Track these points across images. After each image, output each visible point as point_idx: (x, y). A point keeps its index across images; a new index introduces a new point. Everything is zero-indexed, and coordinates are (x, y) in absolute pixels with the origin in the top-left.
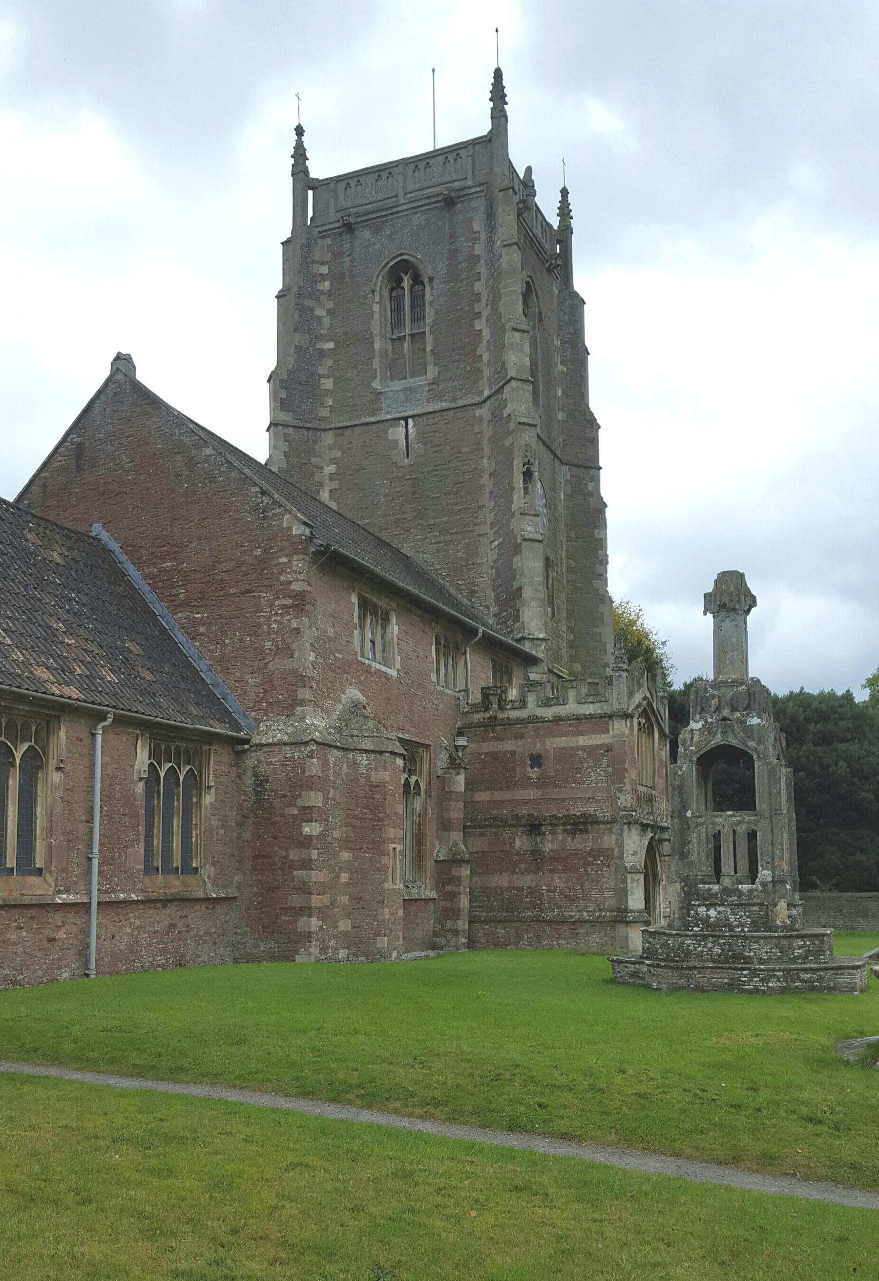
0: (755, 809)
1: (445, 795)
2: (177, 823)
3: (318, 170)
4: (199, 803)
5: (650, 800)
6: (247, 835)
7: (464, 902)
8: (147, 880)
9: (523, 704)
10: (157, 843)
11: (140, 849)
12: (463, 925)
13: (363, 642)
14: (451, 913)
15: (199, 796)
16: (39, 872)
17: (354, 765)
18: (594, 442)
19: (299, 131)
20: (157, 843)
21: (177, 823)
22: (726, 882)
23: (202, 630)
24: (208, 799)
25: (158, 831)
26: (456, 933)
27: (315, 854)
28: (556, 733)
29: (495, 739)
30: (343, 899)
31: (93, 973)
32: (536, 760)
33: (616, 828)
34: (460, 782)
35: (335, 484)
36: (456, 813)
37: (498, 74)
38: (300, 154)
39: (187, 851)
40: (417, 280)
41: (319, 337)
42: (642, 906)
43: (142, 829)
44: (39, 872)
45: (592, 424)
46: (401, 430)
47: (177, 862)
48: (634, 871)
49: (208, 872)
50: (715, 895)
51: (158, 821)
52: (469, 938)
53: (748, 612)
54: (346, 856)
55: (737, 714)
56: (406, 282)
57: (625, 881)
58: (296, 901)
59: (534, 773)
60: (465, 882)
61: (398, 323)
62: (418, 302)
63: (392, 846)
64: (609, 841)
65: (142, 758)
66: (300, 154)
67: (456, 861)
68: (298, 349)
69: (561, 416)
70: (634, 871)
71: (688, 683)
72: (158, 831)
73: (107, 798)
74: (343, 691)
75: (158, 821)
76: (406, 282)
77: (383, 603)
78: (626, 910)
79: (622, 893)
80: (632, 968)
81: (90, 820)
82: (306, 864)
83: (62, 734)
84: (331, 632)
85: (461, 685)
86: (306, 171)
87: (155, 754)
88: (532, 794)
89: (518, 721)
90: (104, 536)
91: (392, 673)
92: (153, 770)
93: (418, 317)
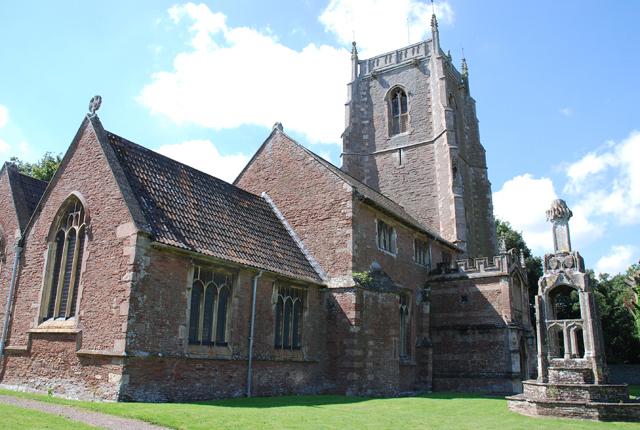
0: (580, 318)
1: (421, 315)
2: (291, 325)
3: (361, 57)
4: (301, 316)
5: (520, 317)
6: (324, 332)
7: (430, 368)
8: (276, 351)
9: (479, 271)
10: (282, 333)
11: (273, 335)
12: (429, 378)
13: (379, 241)
14: (424, 372)
15: (302, 312)
16: (226, 345)
17: (375, 299)
18: (484, 157)
19: (354, 44)
20: (282, 333)
21: (291, 325)
22: (566, 356)
23: (306, 236)
24: (306, 314)
25: (282, 327)
26: (426, 382)
27: (356, 342)
28: (369, 391)
29: (445, 287)
30: (370, 364)
31: (249, 393)
32: (465, 298)
33: (505, 331)
34: (427, 309)
35: (369, 178)
36: (426, 323)
37: (434, 16)
38: (355, 52)
39: (296, 338)
40: (403, 94)
41: (363, 119)
42: (519, 370)
43: (274, 326)
44: (226, 345)
45: (482, 150)
46: (397, 154)
47: (291, 344)
48: (514, 352)
49: (305, 350)
50: (562, 364)
51: (282, 323)
52: (433, 385)
53: (568, 219)
54: (371, 343)
55: (568, 270)
56: (399, 96)
57: (510, 357)
58: (347, 364)
59: (463, 304)
60: (431, 357)
61: (396, 111)
62: (404, 105)
63: (393, 339)
64: (501, 338)
65: (275, 294)
66: (355, 52)
67: (426, 345)
68: (354, 124)
69: (468, 147)
70: (514, 352)
71: (601, 193)
72: (282, 327)
73: (258, 312)
74: (370, 264)
75: (282, 323)
76: (399, 96)
77: (390, 222)
78: (512, 373)
79: (510, 363)
80: (520, 403)
81: (250, 322)
82: (352, 346)
83: (239, 280)
84: (365, 236)
85: (427, 262)
86: (357, 57)
87: (282, 292)
88: (461, 314)
89: (456, 279)
90: (266, 196)
91: (395, 256)
92: (280, 299)
93: (404, 110)
